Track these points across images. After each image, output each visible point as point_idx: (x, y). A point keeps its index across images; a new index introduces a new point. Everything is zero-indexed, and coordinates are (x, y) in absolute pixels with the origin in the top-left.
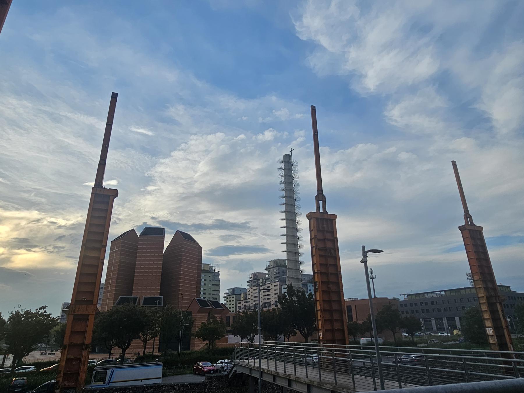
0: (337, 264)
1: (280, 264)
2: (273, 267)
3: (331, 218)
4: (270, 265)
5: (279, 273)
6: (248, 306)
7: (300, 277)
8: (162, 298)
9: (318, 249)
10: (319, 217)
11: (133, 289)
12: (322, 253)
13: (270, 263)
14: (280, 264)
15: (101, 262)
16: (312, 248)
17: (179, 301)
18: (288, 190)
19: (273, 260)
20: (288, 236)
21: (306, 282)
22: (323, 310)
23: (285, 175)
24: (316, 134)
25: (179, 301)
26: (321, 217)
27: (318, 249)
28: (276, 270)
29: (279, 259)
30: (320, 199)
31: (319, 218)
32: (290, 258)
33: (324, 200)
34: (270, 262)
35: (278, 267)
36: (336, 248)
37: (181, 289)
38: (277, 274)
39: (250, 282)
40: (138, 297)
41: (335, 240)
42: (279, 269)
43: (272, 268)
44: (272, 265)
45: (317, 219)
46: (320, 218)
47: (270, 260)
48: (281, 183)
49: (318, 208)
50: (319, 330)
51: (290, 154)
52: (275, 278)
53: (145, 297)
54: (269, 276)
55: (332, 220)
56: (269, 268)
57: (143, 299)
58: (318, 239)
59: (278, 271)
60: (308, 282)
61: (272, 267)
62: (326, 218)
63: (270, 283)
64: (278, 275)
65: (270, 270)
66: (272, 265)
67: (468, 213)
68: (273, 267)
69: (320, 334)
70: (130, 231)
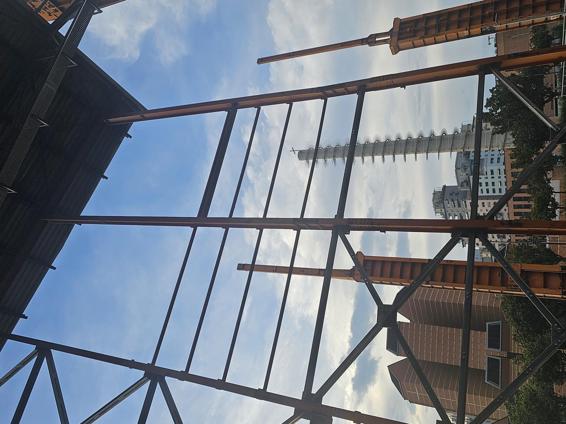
0: (459, 10)
1: (441, 198)
2: (444, 208)
3: (399, 24)
4: (440, 213)
5: (453, 201)
6: (500, 247)
7: (464, 134)
8: (489, 323)
9: (438, 32)
10: (397, 37)
11: (474, 368)
12: (444, 28)
13: (439, 213)
14: (441, 198)
15: (451, 262)
16: (436, 43)
17: (493, 306)
18: (345, 152)
19: (433, 209)
20: (406, 151)
21: (467, 161)
22: (520, 17)
23: (324, 158)
24: (291, 54)
25: (493, 306)
26: (397, 35)
27: (438, 33)
28: (449, 204)
29: (433, 200)
30: (374, 40)
31: (398, 37)
32: (437, 148)
33: (374, 36)
34: (436, 213)
35: (445, 202)
36: (437, 14)
37: (476, 304)
38: (454, 204)
39: (464, 242)
40: (487, 356)
41: (427, 16)
42: (447, 200)
43: (445, 210)
44: (441, 210)
45: (399, 39)
46: (398, 36)
47: (434, 212)
48: (335, 163)
49: (385, 42)
50: (547, 21)
51: (297, 152)
52: (459, 206)
53: (487, 346)
54: (456, 214)
55: (400, 22)
56: (444, 214)
57: (490, 349)
58: (425, 35)
59: (450, 202)
60: (467, 159)
61: (443, 210)
62: (398, 29)
63: (467, 213)
64: (456, 202)
65: (447, 213)
66: (441, 210)
67: (366, 40)
68: (444, 208)
69: (552, 19)
70: (389, 370)
